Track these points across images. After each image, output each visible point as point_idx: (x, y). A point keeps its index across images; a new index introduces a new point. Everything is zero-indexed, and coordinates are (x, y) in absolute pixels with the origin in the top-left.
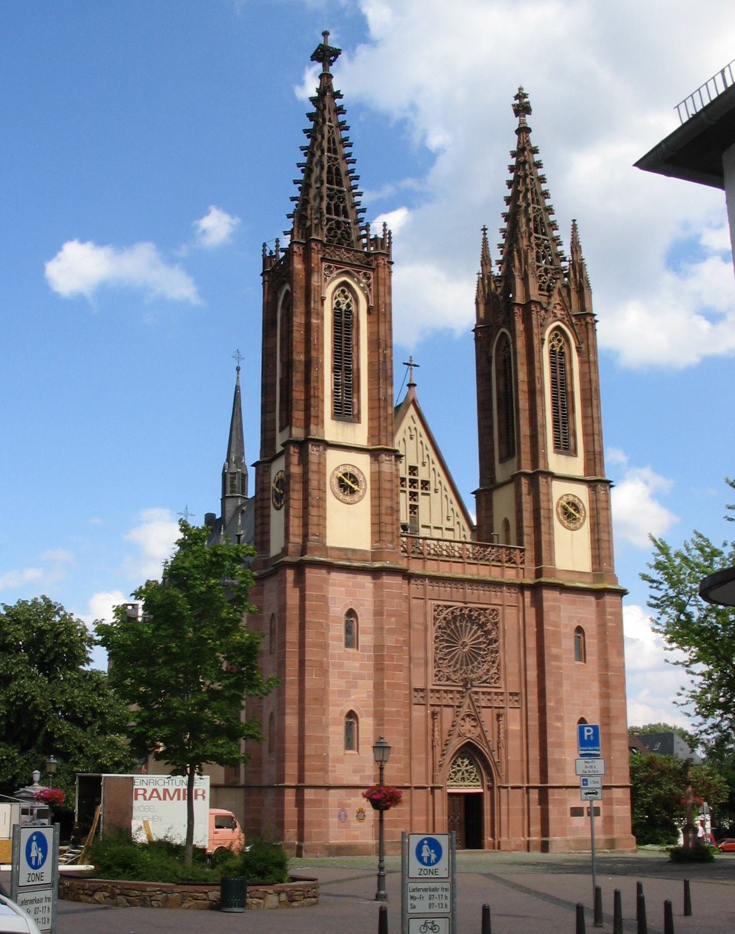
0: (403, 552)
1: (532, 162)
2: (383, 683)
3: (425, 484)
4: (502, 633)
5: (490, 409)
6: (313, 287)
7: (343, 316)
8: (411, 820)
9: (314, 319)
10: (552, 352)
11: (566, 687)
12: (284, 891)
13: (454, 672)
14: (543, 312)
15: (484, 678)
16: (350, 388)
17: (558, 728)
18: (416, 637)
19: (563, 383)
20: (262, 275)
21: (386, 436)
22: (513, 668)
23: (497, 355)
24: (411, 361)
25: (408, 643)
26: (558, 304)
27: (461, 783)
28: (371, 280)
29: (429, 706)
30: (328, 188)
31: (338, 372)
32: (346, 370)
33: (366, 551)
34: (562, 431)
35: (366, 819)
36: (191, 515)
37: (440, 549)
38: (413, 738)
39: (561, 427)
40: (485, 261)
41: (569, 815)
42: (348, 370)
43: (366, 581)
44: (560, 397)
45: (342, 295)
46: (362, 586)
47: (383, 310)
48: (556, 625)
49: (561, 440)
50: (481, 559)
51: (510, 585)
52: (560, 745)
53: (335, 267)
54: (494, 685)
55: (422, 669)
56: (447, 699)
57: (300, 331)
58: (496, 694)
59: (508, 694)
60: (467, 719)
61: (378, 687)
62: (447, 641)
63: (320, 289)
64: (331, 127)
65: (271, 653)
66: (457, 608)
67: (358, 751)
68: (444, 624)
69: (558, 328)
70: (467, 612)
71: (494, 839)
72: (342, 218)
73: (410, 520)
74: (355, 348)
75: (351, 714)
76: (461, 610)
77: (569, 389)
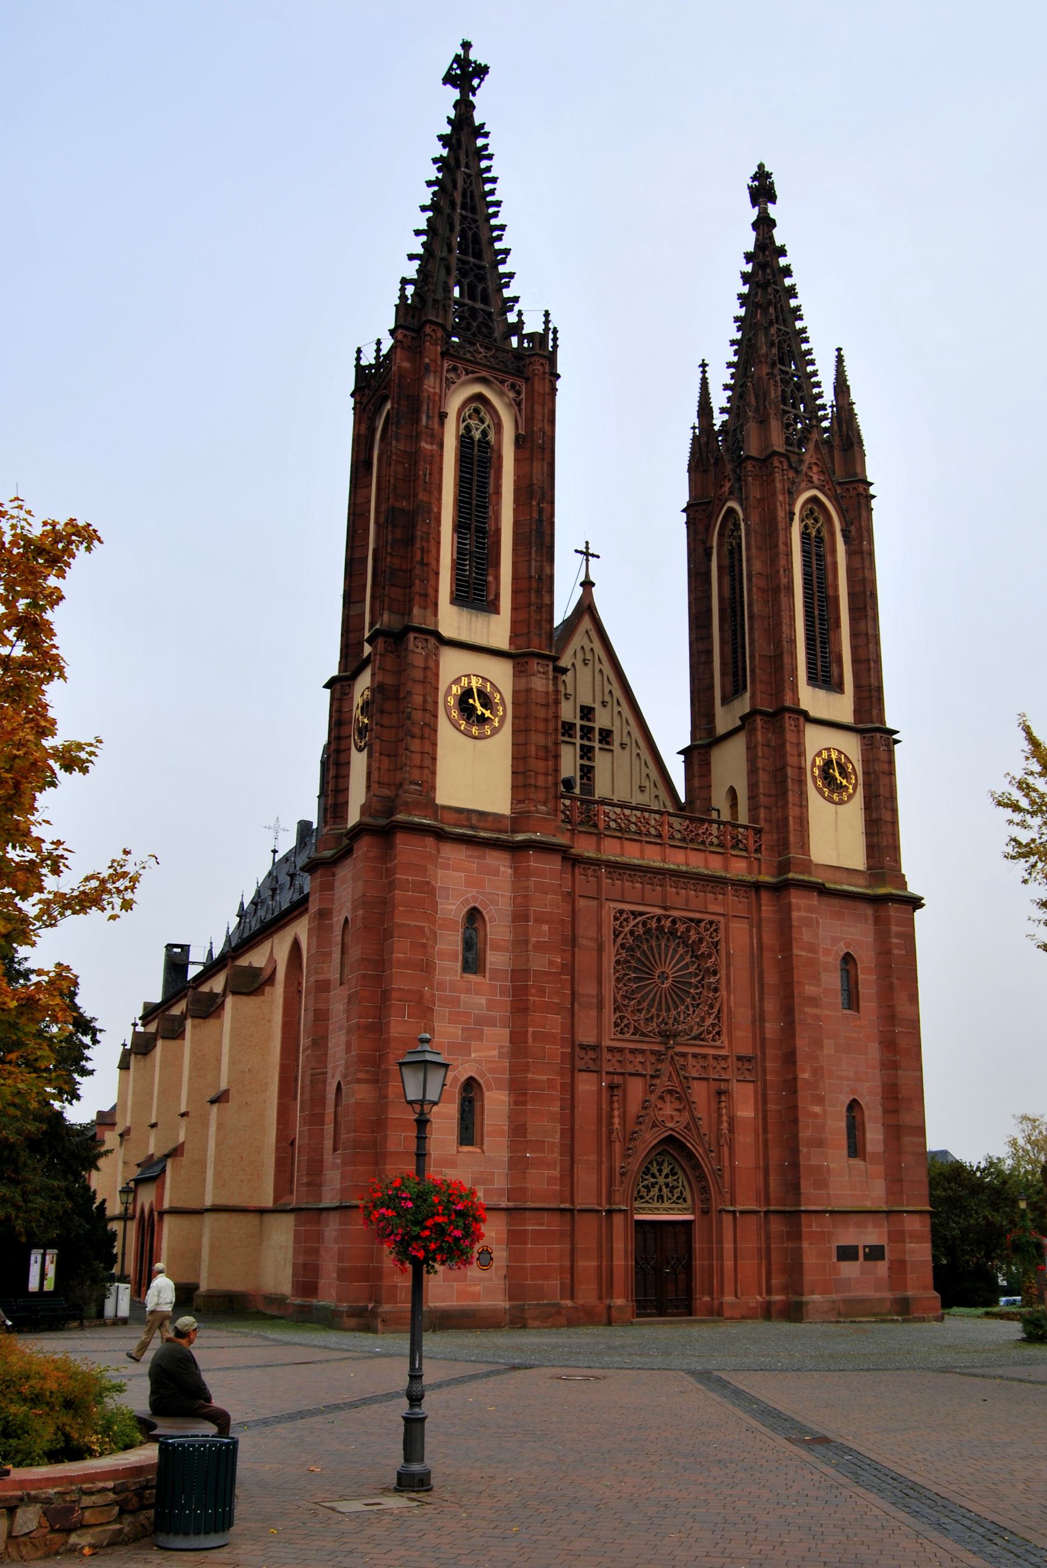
0: (563, 821)
1: (776, 268)
2: (527, 1031)
3: (606, 736)
4: (724, 961)
5: (709, 626)
6: (425, 394)
7: (476, 449)
8: (572, 1266)
9: (426, 442)
10: (805, 535)
11: (829, 1049)
12: (33, 1500)
13: (647, 1019)
14: (791, 474)
15: (695, 1032)
16: (483, 559)
17: (816, 1115)
18: (585, 960)
19: (822, 583)
20: (352, 395)
21: (540, 635)
22: (743, 1015)
23: (720, 546)
24: (587, 548)
25: (570, 969)
26: (815, 464)
27: (658, 1205)
28: (523, 396)
29: (604, 1074)
30: (459, 259)
31: (466, 534)
32: (476, 531)
33: (503, 816)
34: (819, 654)
35: (495, 1264)
36: (284, 830)
37: (626, 822)
38: (577, 1127)
39: (819, 649)
40: (705, 409)
41: (835, 1260)
42: (482, 532)
43: (500, 863)
44: (816, 603)
45: (475, 416)
46: (496, 873)
47: (540, 442)
48: (813, 948)
49: (819, 667)
50: (692, 840)
51: (739, 884)
52: (819, 1143)
53: (466, 370)
54: (713, 1043)
55: (594, 1013)
56: (636, 1064)
57: (403, 463)
58: (716, 1057)
59: (735, 1059)
60: (668, 1098)
61: (518, 1039)
62: (636, 969)
63: (440, 399)
64: (469, 176)
65: (341, 984)
66: (653, 917)
67: (482, 1148)
68: (631, 941)
69: (814, 499)
70: (668, 924)
71: (713, 1299)
72: (479, 305)
73: (581, 788)
74: (494, 497)
75: (470, 1085)
76: (659, 920)
77: (831, 592)
